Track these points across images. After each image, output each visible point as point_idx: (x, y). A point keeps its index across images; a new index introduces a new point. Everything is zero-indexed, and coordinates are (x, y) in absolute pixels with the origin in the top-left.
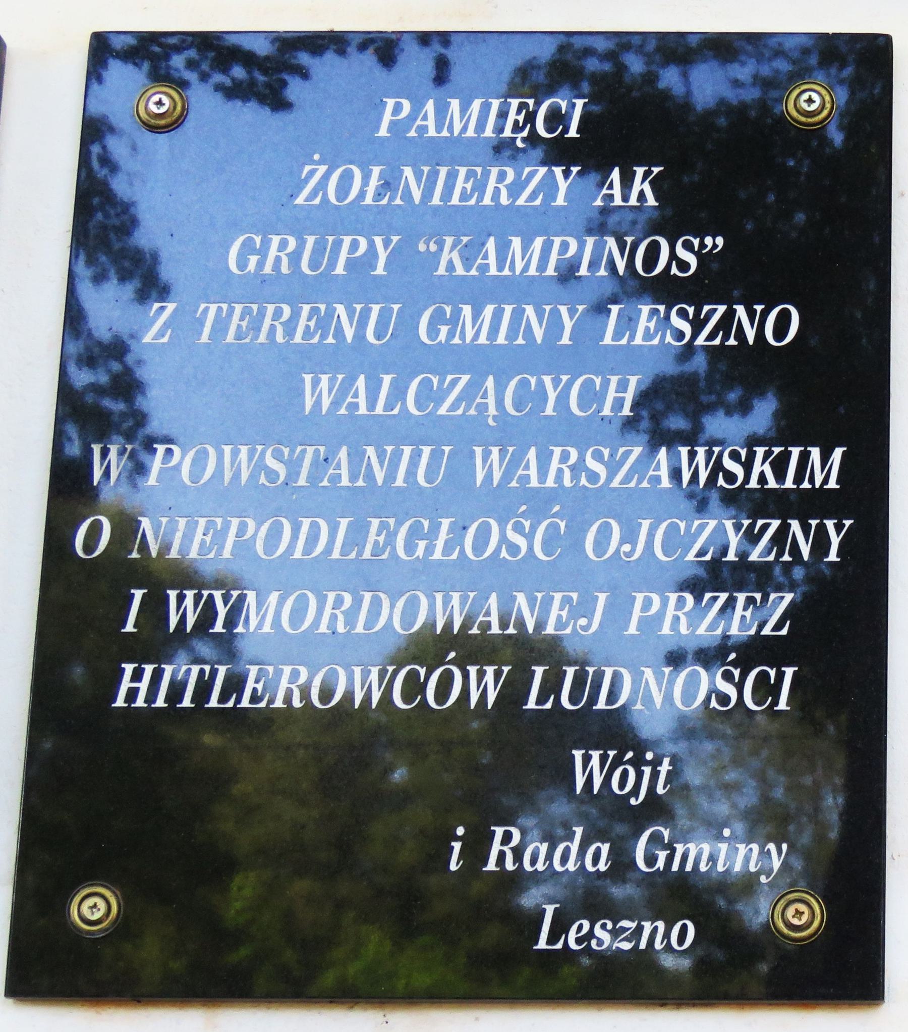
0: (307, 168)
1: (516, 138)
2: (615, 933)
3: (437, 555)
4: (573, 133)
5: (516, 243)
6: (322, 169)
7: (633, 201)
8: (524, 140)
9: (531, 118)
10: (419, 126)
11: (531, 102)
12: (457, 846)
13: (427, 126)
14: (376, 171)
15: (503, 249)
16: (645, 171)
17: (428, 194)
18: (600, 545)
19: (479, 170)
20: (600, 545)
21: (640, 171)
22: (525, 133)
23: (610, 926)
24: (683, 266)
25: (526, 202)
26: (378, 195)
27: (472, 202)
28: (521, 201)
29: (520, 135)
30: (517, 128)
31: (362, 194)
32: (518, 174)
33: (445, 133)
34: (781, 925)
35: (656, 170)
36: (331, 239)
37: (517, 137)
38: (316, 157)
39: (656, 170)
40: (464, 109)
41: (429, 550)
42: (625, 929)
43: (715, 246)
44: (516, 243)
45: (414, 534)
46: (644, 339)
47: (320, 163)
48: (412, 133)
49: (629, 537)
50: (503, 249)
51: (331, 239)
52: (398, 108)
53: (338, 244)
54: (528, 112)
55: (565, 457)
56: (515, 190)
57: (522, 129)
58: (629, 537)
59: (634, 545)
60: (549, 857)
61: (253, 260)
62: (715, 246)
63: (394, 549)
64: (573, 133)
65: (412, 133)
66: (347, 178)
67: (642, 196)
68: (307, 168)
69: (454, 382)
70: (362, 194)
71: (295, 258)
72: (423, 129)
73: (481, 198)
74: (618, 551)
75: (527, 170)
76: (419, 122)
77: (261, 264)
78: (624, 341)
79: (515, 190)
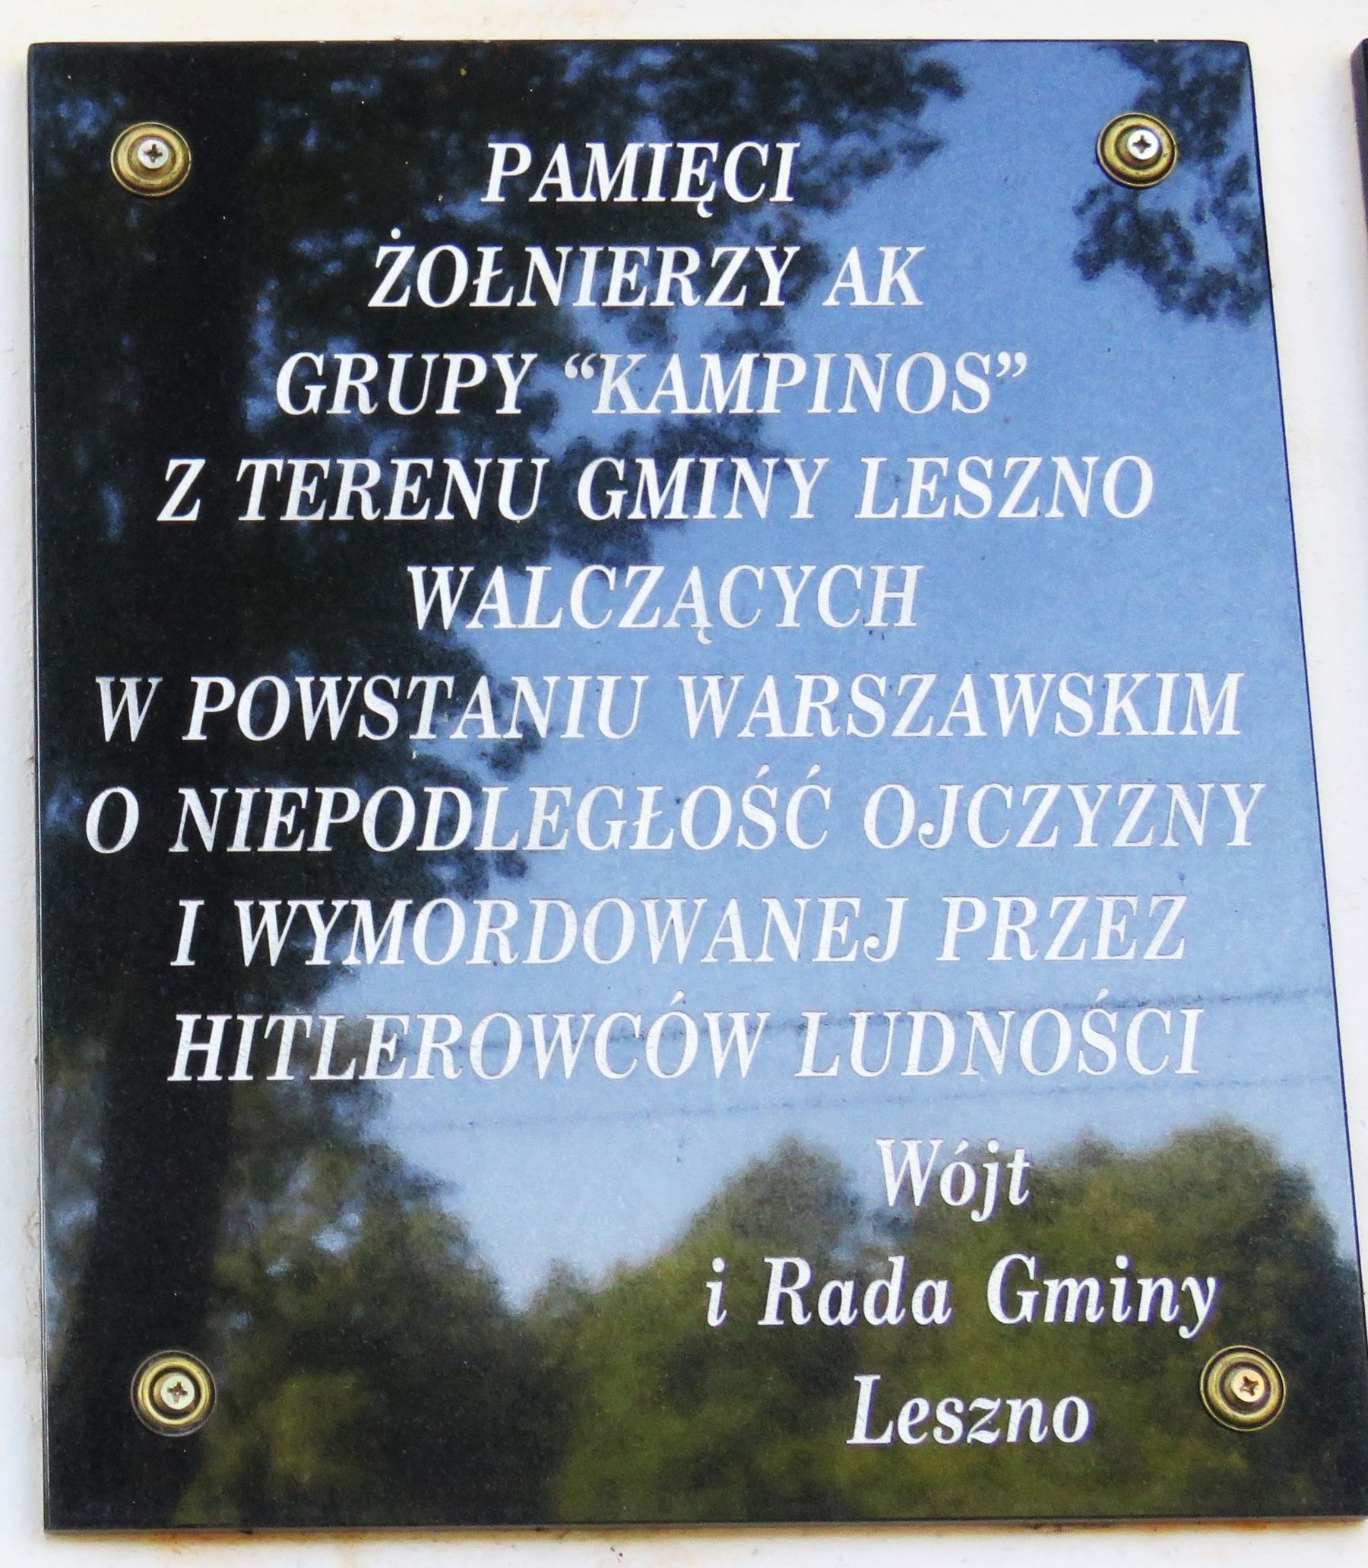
0: (384, 251)
1: (698, 203)
3: (641, 842)
5: (598, 152)
6: (406, 252)
7: (884, 299)
11: (713, 148)
12: (716, 1288)
14: (489, 253)
15: (579, 160)
18: (887, 825)
20: (887, 825)
21: (890, 253)
22: (709, 196)
24: (970, 397)
26: (495, 293)
30: (696, 189)
31: (471, 291)
32: (706, 257)
33: (588, 197)
35: (914, 251)
37: (698, 203)
38: (396, 234)
39: (914, 251)
40: (614, 158)
41: (629, 834)
43: (1014, 367)
44: (598, 152)
45: (603, 810)
47: (400, 242)
48: (538, 197)
49: (930, 811)
50: (579, 160)
52: (512, 159)
53: (442, 368)
55: (819, 691)
57: (704, 190)
58: (930, 811)
59: (938, 822)
60: (857, 1302)
61: (315, 392)
62: (1014, 367)
63: (574, 833)
65: (538, 197)
67: (896, 290)
70: (471, 291)
71: (378, 389)
72: (553, 190)
74: (914, 835)
76: (546, 180)
77: (327, 399)
78: (891, 514)
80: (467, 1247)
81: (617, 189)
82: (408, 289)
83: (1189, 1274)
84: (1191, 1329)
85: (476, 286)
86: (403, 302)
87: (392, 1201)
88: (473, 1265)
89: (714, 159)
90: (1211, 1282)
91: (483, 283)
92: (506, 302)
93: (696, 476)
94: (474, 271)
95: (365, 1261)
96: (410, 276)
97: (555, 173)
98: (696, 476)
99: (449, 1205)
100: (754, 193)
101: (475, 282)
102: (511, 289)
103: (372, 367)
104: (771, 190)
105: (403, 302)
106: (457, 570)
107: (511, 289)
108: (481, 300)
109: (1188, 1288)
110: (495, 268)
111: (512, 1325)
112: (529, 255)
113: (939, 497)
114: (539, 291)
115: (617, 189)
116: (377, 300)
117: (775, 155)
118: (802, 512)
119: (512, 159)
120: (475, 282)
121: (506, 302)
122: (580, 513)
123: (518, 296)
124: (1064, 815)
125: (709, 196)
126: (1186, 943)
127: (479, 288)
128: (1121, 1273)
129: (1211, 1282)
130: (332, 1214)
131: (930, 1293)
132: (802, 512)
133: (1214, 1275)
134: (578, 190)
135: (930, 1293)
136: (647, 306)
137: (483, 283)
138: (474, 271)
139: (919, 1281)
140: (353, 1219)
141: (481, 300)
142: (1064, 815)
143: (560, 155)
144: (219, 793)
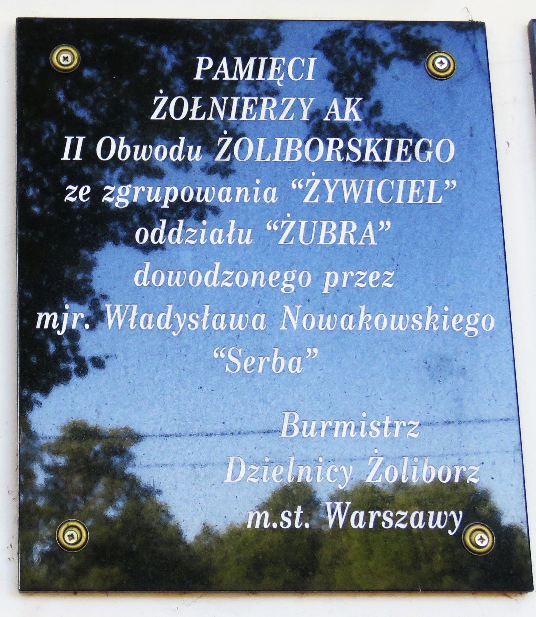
1: (277, 81)
2: (395, 519)
4: (310, 78)
5: (239, 60)
6: (165, 99)
8: (281, 81)
9: (285, 68)
10: (219, 73)
13: (224, 74)
14: (197, 99)
16: (352, 100)
17: (228, 112)
19: (256, 99)
22: (282, 78)
23: (392, 514)
25: (285, 118)
26: (199, 114)
27: (254, 118)
28: (282, 118)
29: (278, 80)
31: (189, 114)
32: (279, 102)
33: (235, 78)
34: (71, 524)
36: (315, 222)
37: (277, 81)
38: (161, 91)
40: (244, 64)
42: (400, 516)
43: (271, 224)
44: (239, 60)
46: (247, 117)
48: (215, 78)
51: (315, 222)
52: (206, 62)
54: (282, 66)
56: (279, 110)
57: (280, 76)
64: (310, 78)
65: (215, 78)
66: (179, 104)
68: (221, 139)
69: (287, 102)
70: (189, 114)
72: (221, 76)
73: (258, 116)
75: (284, 99)
76: (218, 71)
79: (279, 110)
80: (169, 517)
81: (246, 75)
82: (165, 113)
83: (453, 510)
84: (452, 531)
85: (192, 111)
86: (164, 118)
87: (137, 498)
88: (172, 523)
89: (411, 145)
90: (461, 513)
91: (194, 111)
92: (203, 118)
93: (257, 64)
94: (191, 106)
95: (125, 520)
96: (166, 108)
97: (222, 69)
98: (257, 64)
99: (160, 499)
100: (298, 78)
101: (191, 110)
102: (205, 113)
103: (334, 226)
104: (306, 76)
105: (164, 118)
106: (310, 222)
107: (205, 113)
108: (193, 117)
109: (452, 515)
110: (199, 105)
111: (188, 548)
112: (212, 100)
113: (421, 195)
114: (216, 114)
115: (246, 75)
116: (154, 117)
117: (308, 63)
118: (330, 200)
119: (206, 62)
120: (191, 110)
121: (203, 118)
122: (118, 158)
123: (207, 116)
124: (322, 190)
125: (282, 78)
126: (295, 238)
127: (193, 113)
128: (257, 186)
129: (461, 513)
130: (111, 502)
131: (357, 516)
132: (330, 200)
133: (462, 510)
134: (231, 75)
135: (357, 516)
136: (256, 120)
137: (194, 111)
138: (191, 106)
139: (353, 511)
140: (120, 504)
141: (193, 117)
142: (322, 190)
143: (224, 62)
144: (226, 99)
